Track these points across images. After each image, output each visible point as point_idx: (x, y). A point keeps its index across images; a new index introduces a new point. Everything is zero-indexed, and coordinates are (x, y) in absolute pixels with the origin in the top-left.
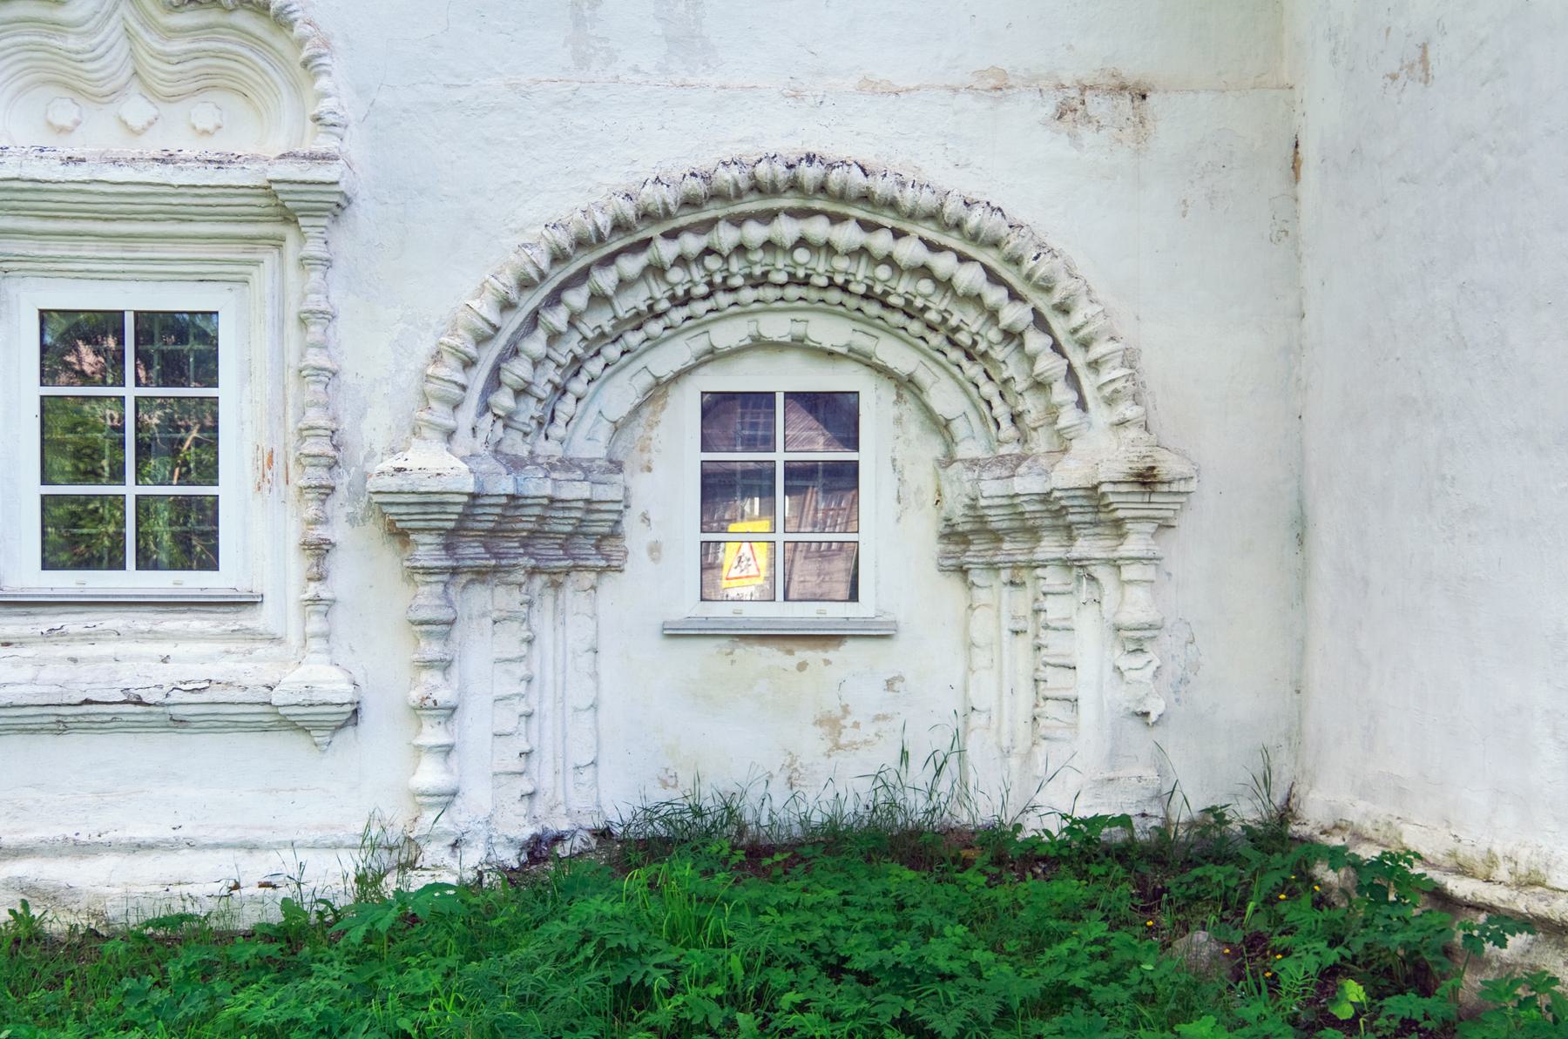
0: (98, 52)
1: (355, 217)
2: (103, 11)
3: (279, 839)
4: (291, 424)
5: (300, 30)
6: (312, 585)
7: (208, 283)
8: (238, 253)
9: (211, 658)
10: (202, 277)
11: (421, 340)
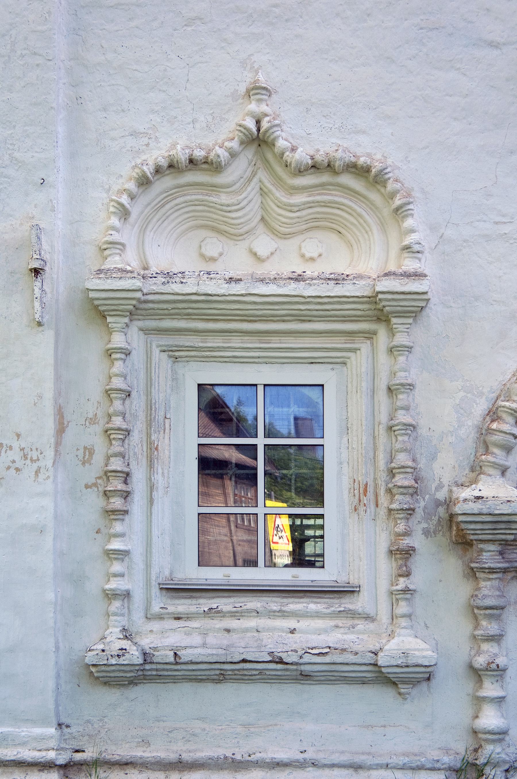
0: (242, 205)
1: (428, 317)
2: (245, 177)
3: (377, 762)
4: (382, 464)
5: (391, 186)
6: (402, 580)
7: (318, 365)
8: (342, 343)
9: (325, 631)
10: (313, 361)
11: (477, 404)
